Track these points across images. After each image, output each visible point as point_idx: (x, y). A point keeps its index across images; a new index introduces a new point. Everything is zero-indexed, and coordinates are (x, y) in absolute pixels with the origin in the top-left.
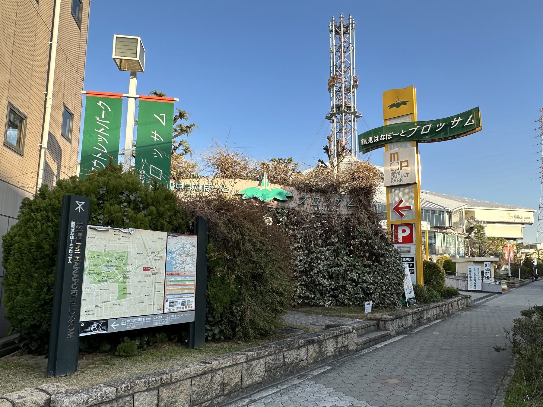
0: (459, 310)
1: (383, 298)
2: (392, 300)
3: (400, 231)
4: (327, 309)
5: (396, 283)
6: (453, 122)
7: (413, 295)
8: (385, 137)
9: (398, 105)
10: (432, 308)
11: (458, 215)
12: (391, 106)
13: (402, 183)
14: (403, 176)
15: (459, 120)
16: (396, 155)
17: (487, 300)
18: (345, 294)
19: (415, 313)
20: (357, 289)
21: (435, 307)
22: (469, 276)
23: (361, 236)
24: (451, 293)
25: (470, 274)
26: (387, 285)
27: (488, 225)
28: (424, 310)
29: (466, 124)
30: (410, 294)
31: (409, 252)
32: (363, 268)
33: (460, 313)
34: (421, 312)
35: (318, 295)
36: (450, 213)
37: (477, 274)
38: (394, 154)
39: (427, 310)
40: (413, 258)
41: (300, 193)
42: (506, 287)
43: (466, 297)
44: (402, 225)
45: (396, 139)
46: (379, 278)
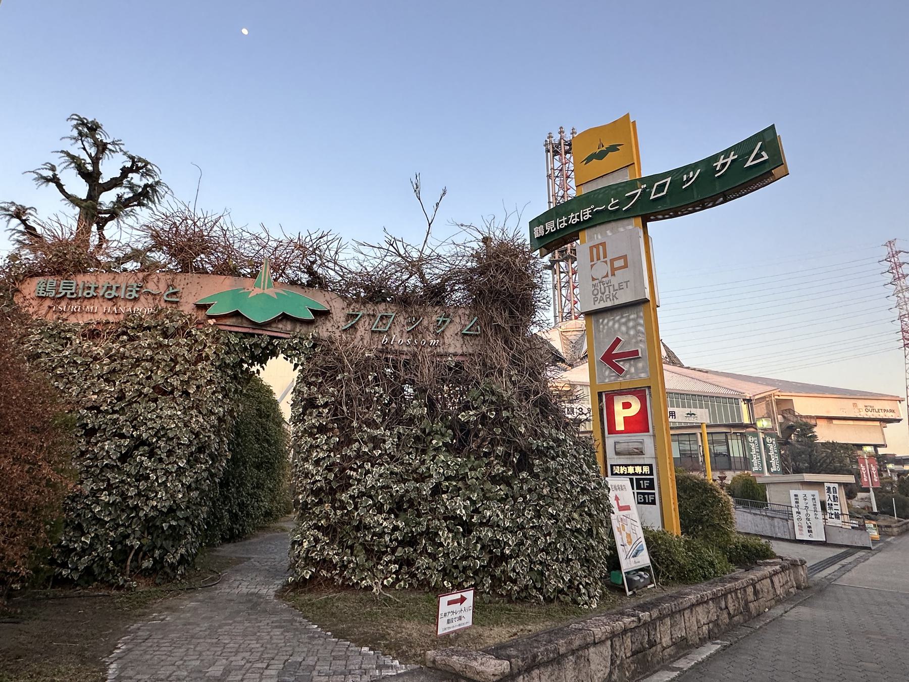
0: (779, 601)
1: (541, 573)
2: (567, 578)
3: (618, 407)
4: (373, 601)
5: (578, 531)
6: (719, 164)
7: (644, 559)
8: (579, 217)
9: (600, 156)
10: (692, 606)
11: (763, 405)
12: (589, 160)
13: (617, 302)
14: (616, 287)
15: (732, 158)
16: (601, 247)
17: (845, 569)
18: (433, 557)
19: (625, 631)
20: (468, 543)
21: (699, 603)
22: (794, 510)
23: (484, 402)
24: (751, 555)
25: (798, 507)
26: (549, 534)
27: (819, 422)
28: (661, 618)
29: (748, 164)
30: (634, 558)
31: (642, 453)
32: (488, 486)
33: (778, 611)
34: (650, 625)
35: (361, 558)
36: (748, 401)
37: (811, 508)
38: (597, 246)
39: (672, 614)
40: (651, 466)
41: (349, 305)
42: (875, 534)
43: (794, 564)
44: (621, 393)
45: (600, 219)
46: (529, 514)
